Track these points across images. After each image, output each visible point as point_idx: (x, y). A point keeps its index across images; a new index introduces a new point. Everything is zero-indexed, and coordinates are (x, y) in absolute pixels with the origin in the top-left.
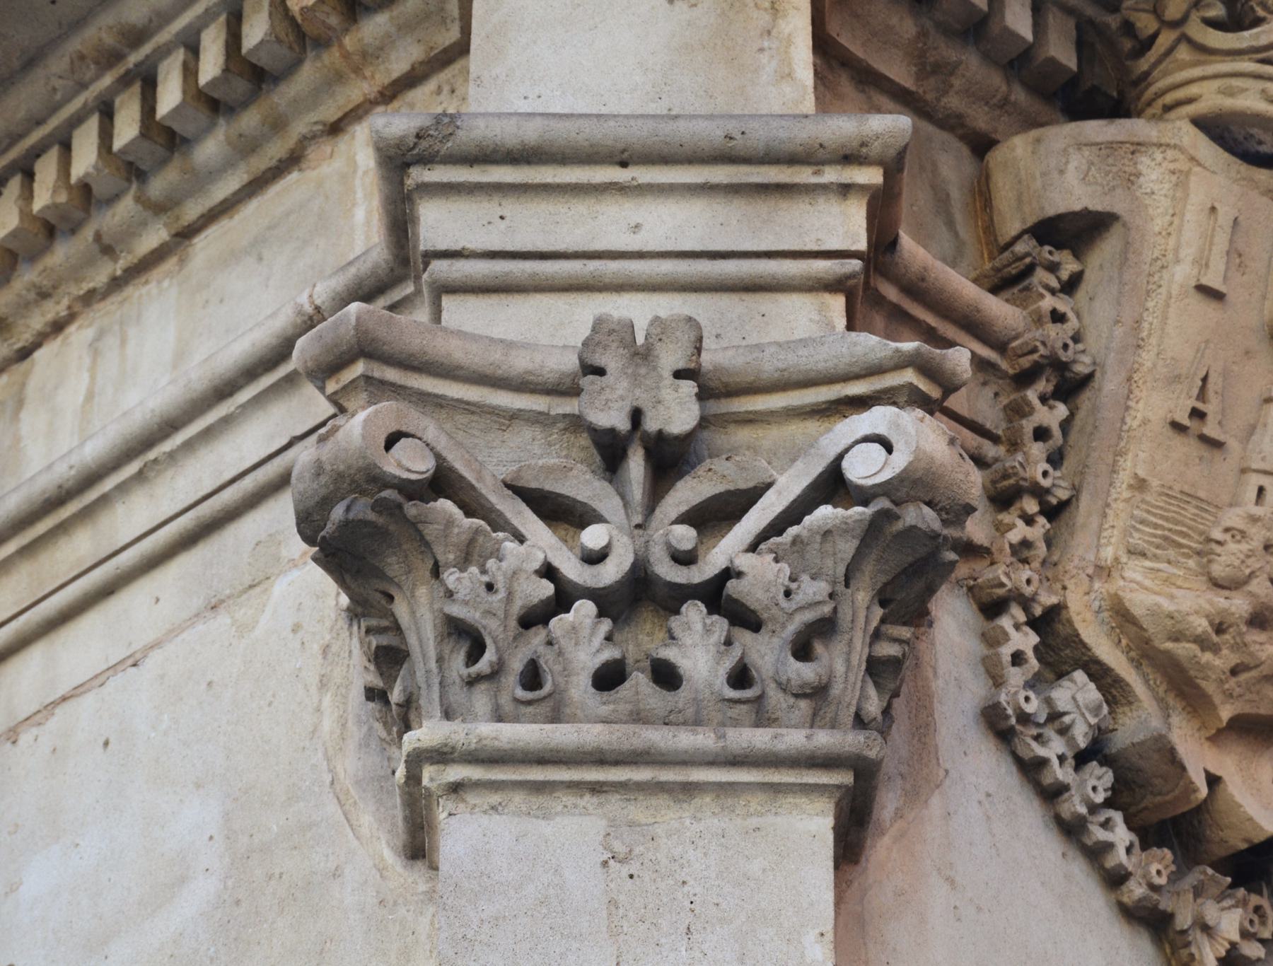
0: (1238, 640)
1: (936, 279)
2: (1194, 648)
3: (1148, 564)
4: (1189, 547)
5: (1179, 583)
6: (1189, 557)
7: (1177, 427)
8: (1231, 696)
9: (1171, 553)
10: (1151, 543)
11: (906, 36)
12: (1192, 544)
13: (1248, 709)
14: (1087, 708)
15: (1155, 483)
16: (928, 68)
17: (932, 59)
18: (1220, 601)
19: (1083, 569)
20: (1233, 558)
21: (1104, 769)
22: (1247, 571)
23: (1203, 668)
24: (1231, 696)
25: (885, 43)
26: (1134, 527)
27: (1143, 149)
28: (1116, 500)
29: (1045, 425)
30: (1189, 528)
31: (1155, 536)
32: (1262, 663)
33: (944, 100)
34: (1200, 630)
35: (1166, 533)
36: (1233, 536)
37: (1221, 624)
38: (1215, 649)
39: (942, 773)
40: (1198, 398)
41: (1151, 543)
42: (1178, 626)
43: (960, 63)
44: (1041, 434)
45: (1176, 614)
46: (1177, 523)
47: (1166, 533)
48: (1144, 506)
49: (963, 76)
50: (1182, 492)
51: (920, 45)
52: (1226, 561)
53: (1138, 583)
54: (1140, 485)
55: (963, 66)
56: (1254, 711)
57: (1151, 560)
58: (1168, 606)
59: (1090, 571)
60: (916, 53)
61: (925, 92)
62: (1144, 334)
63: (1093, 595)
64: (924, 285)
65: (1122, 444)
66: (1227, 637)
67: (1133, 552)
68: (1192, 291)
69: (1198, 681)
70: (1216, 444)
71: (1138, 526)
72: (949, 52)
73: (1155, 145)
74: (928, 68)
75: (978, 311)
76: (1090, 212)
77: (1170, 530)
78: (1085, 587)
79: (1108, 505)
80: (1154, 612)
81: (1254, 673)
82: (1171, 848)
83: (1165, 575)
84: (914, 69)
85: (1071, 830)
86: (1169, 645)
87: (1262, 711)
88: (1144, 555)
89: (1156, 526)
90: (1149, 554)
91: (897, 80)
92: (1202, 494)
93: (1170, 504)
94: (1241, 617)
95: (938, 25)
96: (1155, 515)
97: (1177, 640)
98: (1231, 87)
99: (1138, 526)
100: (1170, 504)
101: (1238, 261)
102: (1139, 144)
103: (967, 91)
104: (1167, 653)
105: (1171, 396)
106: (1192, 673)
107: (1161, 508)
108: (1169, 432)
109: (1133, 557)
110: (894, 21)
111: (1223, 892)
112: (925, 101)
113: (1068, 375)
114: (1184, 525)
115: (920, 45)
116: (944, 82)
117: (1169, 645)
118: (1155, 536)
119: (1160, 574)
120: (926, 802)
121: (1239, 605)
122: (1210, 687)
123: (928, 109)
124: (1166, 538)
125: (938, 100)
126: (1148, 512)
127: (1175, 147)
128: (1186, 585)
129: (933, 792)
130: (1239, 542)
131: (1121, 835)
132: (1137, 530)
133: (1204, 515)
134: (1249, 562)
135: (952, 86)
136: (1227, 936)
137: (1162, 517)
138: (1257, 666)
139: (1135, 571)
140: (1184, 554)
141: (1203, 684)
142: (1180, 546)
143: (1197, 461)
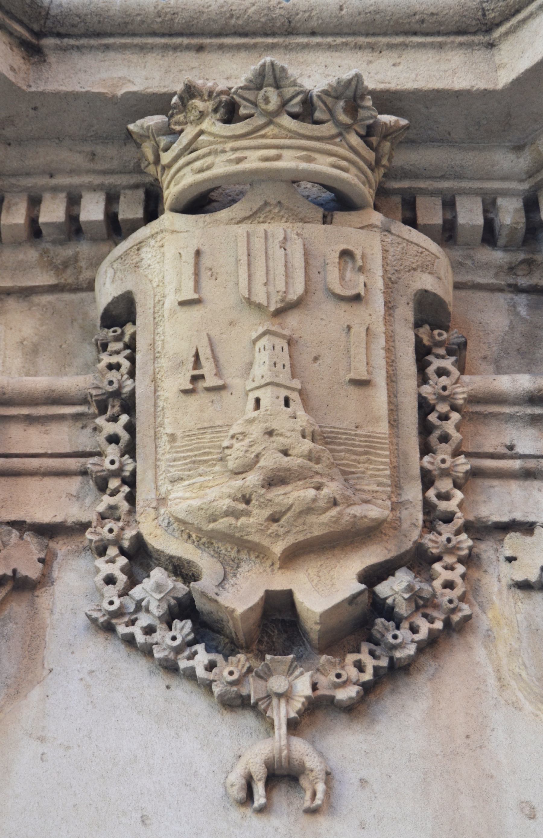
0: (262, 500)
1: (13, 389)
2: (231, 520)
3: (186, 483)
4: (214, 460)
5: (210, 484)
6: (215, 465)
7: (186, 392)
8: (278, 535)
9: (202, 469)
10: (184, 470)
11: (34, 259)
12: (215, 457)
13: (301, 538)
14: (152, 591)
15: (179, 433)
16: (60, 267)
17: (59, 261)
18: (238, 483)
19: (148, 506)
20: (238, 452)
21: (184, 622)
22: (253, 456)
23: (242, 529)
24: (278, 535)
25: (25, 270)
26: (169, 466)
27: (143, 244)
28: (163, 454)
29: (112, 433)
30: (209, 448)
31: (186, 464)
32: (291, 506)
33: (81, 277)
34: (225, 508)
35: (194, 458)
36: (237, 439)
37: (244, 496)
38: (248, 514)
39: (46, 672)
40: (195, 368)
41: (184, 470)
42: (209, 512)
43: (78, 253)
44: (113, 439)
45: (203, 506)
46: (199, 449)
47: (194, 458)
48: (174, 450)
49: (83, 259)
50: (199, 429)
51: (45, 259)
52: (237, 455)
53: (180, 498)
54: (173, 437)
55: (81, 254)
56: (309, 536)
57: (187, 480)
58: (196, 503)
59: (154, 504)
60: (46, 264)
61: (66, 280)
62: (159, 349)
63: (161, 518)
64: (7, 396)
65: (159, 420)
66: (253, 502)
67: (173, 481)
68: (179, 308)
69: (245, 537)
70: (221, 388)
71: (172, 464)
72: (67, 252)
73: (149, 237)
74: (60, 267)
75: (53, 391)
76: (117, 298)
77: (196, 456)
78: (153, 516)
79: (157, 460)
80: (190, 511)
81: (289, 514)
82: (239, 653)
83: (199, 484)
84: (52, 272)
85: (170, 668)
86: (212, 526)
87: (316, 533)
88: (182, 479)
89: (185, 458)
90: (185, 477)
91: (42, 284)
92: (218, 423)
93: (191, 440)
94: (255, 486)
95: (54, 242)
96: (182, 452)
97: (215, 520)
98: (310, 156)
99: (172, 464)
100: (191, 440)
101: (209, 273)
102: (140, 243)
103: (91, 264)
104: (212, 530)
105: (180, 375)
106: (237, 535)
107: (186, 445)
108: (183, 397)
109: (176, 483)
110: (21, 256)
111: (290, 666)
112: (68, 284)
113: (123, 396)
114: (205, 448)
115: (45, 259)
116: (75, 268)
117: (212, 526)
118: (186, 464)
119: (196, 485)
120: (26, 696)
121: (253, 479)
122: (255, 538)
123: (74, 287)
124: (194, 462)
125: (77, 279)
126: (177, 452)
127: (162, 231)
128: (216, 483)
129: (35, 686)
130: (242, 440)
131: (202, 657)
132: (172, 466)
133: (218, 435)
134: (252, 449)
135: (81, 267)
136: (302, 694)
137: (188, 451)
138: (289, 509)
139: (178, 492)
140: (210, 465)
141: (250, 538)
142: (206, 461)
143: (210, 404)
